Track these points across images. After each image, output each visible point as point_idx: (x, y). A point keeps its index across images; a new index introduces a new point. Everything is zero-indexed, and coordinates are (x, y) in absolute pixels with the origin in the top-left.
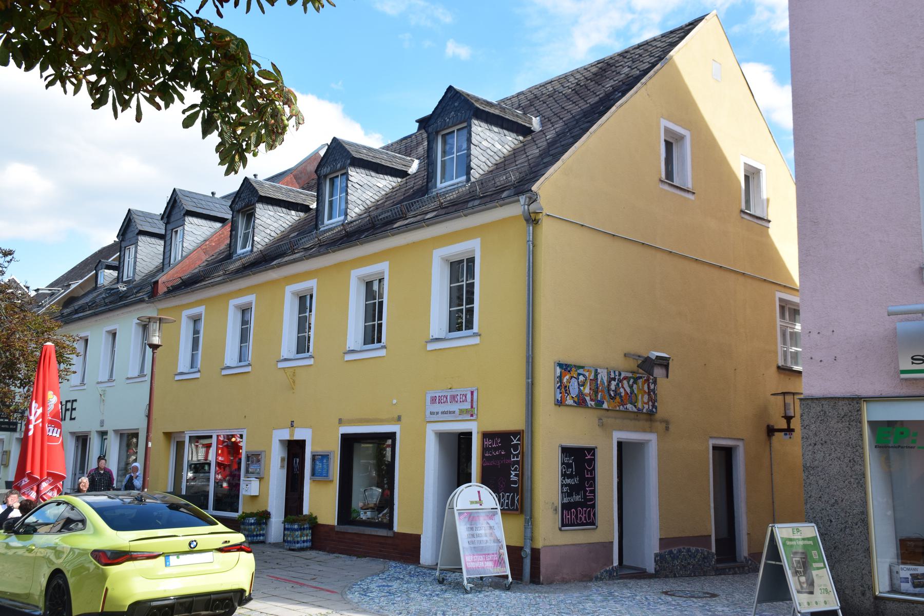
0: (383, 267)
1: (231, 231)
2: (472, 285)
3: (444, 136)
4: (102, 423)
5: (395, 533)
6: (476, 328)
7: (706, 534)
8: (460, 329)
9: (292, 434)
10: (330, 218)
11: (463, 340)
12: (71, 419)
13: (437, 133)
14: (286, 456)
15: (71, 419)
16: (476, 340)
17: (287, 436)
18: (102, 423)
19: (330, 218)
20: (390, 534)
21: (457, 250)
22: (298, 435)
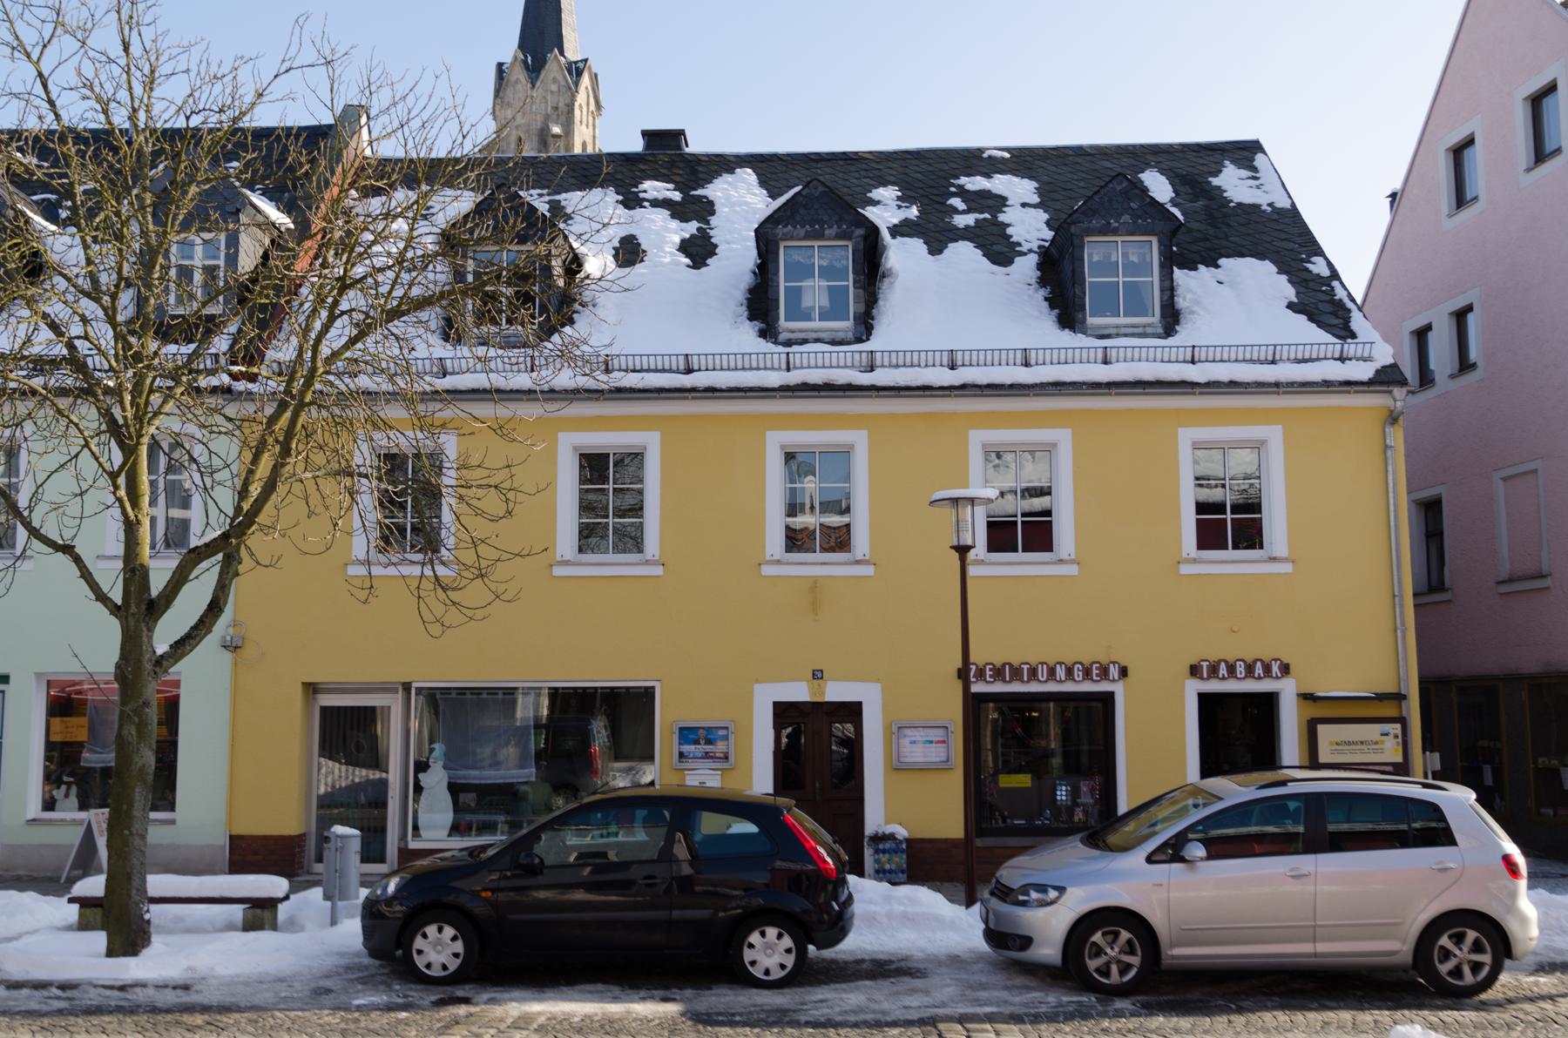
0: (859, 440)
17: (799, 692)
22: (835, 692)
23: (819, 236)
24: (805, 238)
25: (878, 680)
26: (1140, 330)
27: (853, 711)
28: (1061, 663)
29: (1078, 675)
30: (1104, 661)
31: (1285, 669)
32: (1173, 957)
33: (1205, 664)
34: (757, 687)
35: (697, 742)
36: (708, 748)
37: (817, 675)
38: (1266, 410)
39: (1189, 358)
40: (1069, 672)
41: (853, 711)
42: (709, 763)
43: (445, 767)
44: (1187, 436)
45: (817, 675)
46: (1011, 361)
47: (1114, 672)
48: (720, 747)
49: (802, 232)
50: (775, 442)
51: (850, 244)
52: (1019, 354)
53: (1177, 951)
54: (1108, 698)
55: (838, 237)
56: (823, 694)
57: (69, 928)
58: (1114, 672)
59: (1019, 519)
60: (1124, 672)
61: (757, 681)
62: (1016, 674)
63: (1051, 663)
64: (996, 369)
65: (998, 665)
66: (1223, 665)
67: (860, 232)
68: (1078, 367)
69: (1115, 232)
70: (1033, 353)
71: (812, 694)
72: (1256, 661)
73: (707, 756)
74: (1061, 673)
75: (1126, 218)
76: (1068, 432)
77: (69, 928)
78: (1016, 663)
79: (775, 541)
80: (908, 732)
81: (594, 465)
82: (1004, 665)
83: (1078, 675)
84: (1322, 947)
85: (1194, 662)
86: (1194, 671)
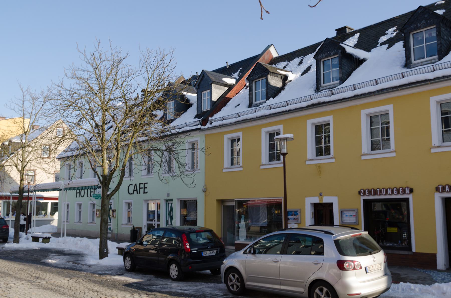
0: (390, 108)
1: (249, 92)
2: (329, 137)
3: (255, 82)
4: (168, 195)
5: (414, 253)
6: (199, 168)
7: (140, 227)
8: (321, 155)
9: (322, 199)
10: (255, 101)
11: (324, 160)
12: (144, 193)
13: (252, 81)
14: (313, 211)
15: (144, 193)
16: (333, 160)
17: (316, 200)
18: (168, 195)
19: (255, 101)
20: (410, 253)
21: (192, 140)
22: (326, 200)
23: (329, 56)
24: (326, 58)
25: (337, 196)
26: (430, 62)
27: (331, 205)
28: (389, 188)
29: (395, 192)
30: (404, 187)
31: (411, 191)
32: (248, 285)
33: (440, 187)
34: (306, 198)
35: (292, 216)
36: (295, 217)
37: (321, 195)
38: (368, 104)
39: (433, 70)
40: (392, 191)
41: (331, 205)
42: (295, 222)
43: (244, 221)
44: (434, 101)
45: (321, 195)
46: (424, 72)
47: (407, 191)
48: (297, 217)
49: (325, 56)
50: (364, 114)
51: (168, 103)
52: (374, 81)
53: (249, 283)
54: (407, 200)
55: (334, 55)
56: (322, 201)
57: (116, 254)
58: (407, 191)
59: (444, 130)
60: (411, 191)
61: (306, 197)
62: (375, 193)
63: (387, 188)
64: (364, 89)
65: (370, 189)
66: (447, 187)
67: (340, 51)
68: (387, 83)
69: (420, 28)
70: (379, 80)
71: (320, 201)
72: (446, 185)
73: (294, 219)
74: (389, 192)
75: (424, 22)
76: (332, 116)
77: (116, 254)
78: (375, 188)
79: (366, 146)
80: (345, 212)
81: (318, 129)
82: (372, 189)
83: (395, 192)
84: (283, 287)
85: (437, 186)
86: (437, 189)
